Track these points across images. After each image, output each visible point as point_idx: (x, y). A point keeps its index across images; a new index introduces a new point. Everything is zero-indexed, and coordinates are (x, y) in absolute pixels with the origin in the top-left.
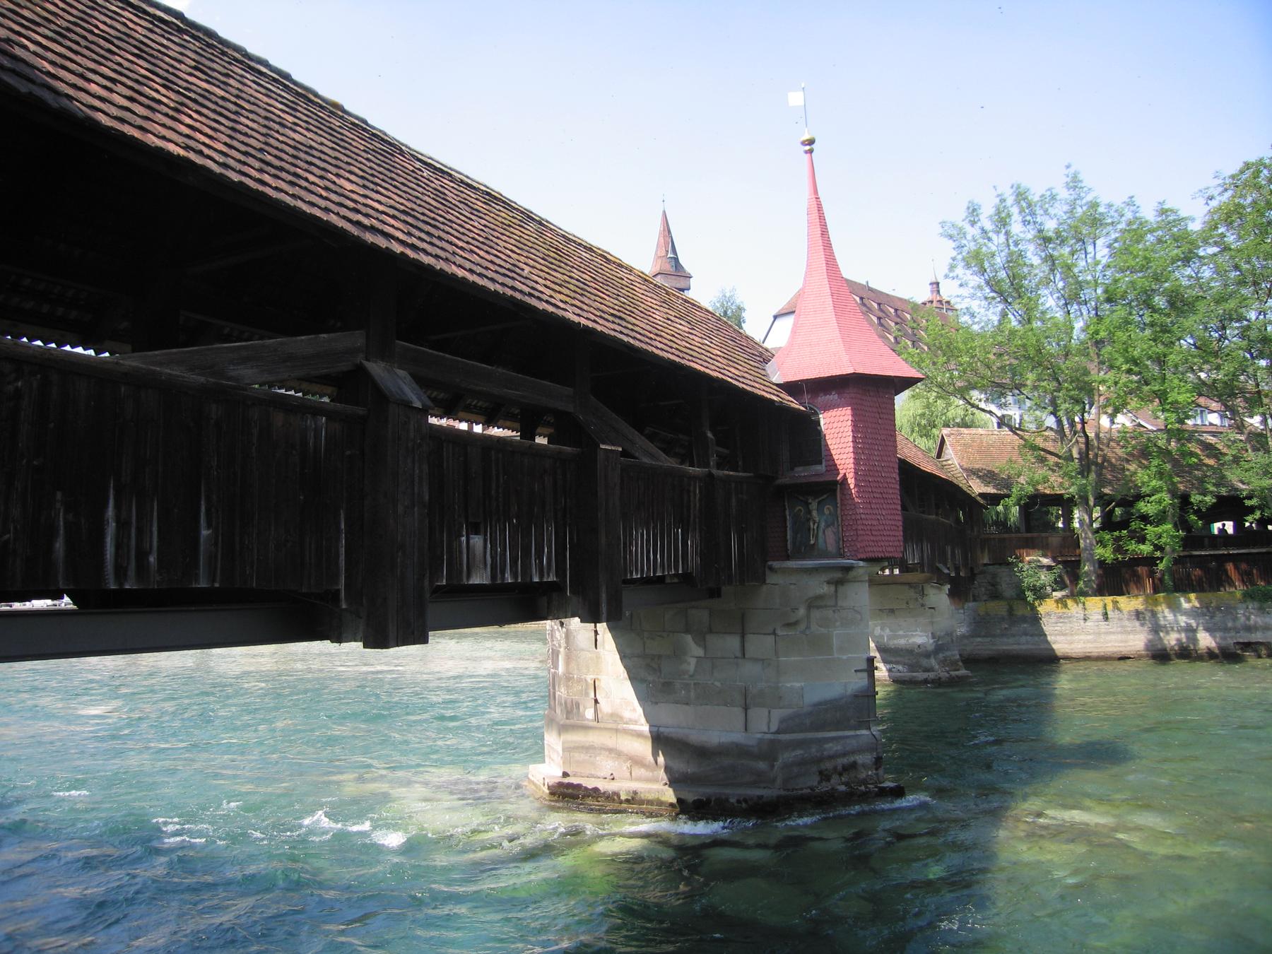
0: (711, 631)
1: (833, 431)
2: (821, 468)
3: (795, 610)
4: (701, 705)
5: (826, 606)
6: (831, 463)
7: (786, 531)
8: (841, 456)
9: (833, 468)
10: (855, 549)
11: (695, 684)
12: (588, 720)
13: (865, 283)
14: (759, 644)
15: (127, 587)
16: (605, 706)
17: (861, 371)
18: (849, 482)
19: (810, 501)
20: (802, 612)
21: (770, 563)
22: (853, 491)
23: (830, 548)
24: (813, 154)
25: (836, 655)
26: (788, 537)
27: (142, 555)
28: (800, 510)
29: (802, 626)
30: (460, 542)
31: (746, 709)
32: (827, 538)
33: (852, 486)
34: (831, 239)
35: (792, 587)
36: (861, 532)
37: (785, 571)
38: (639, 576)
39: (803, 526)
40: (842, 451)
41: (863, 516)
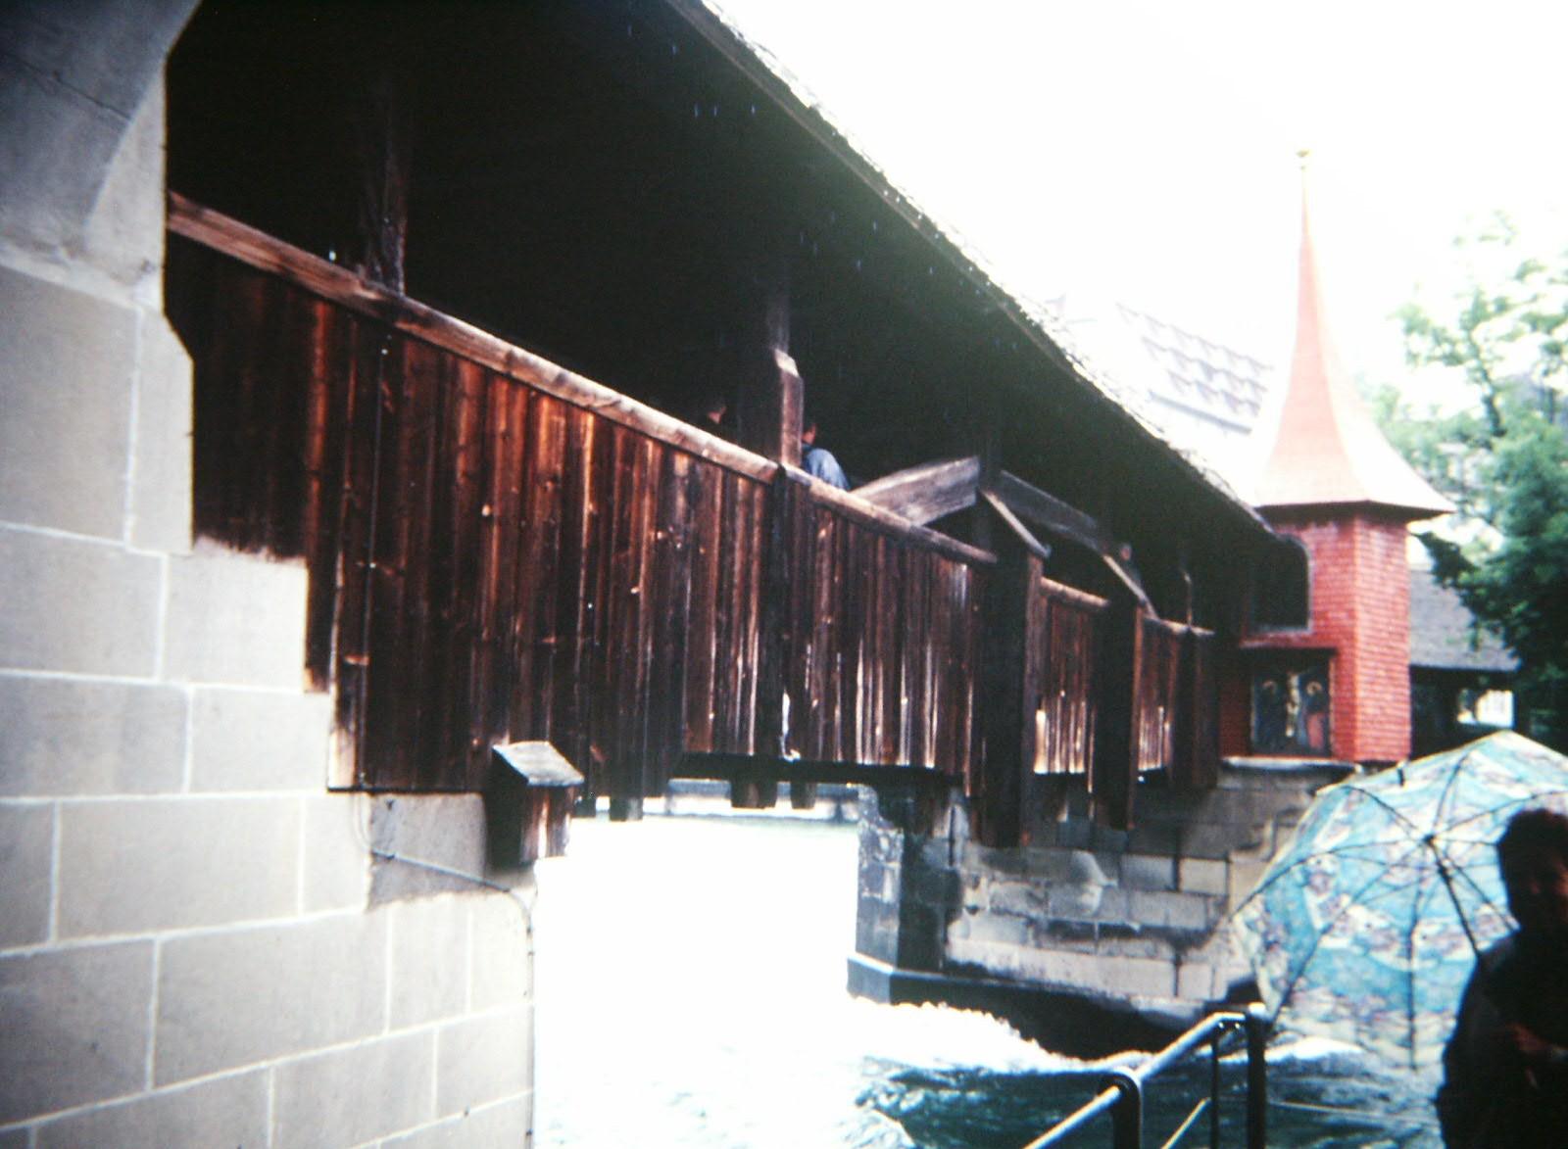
20: (1268, 831)
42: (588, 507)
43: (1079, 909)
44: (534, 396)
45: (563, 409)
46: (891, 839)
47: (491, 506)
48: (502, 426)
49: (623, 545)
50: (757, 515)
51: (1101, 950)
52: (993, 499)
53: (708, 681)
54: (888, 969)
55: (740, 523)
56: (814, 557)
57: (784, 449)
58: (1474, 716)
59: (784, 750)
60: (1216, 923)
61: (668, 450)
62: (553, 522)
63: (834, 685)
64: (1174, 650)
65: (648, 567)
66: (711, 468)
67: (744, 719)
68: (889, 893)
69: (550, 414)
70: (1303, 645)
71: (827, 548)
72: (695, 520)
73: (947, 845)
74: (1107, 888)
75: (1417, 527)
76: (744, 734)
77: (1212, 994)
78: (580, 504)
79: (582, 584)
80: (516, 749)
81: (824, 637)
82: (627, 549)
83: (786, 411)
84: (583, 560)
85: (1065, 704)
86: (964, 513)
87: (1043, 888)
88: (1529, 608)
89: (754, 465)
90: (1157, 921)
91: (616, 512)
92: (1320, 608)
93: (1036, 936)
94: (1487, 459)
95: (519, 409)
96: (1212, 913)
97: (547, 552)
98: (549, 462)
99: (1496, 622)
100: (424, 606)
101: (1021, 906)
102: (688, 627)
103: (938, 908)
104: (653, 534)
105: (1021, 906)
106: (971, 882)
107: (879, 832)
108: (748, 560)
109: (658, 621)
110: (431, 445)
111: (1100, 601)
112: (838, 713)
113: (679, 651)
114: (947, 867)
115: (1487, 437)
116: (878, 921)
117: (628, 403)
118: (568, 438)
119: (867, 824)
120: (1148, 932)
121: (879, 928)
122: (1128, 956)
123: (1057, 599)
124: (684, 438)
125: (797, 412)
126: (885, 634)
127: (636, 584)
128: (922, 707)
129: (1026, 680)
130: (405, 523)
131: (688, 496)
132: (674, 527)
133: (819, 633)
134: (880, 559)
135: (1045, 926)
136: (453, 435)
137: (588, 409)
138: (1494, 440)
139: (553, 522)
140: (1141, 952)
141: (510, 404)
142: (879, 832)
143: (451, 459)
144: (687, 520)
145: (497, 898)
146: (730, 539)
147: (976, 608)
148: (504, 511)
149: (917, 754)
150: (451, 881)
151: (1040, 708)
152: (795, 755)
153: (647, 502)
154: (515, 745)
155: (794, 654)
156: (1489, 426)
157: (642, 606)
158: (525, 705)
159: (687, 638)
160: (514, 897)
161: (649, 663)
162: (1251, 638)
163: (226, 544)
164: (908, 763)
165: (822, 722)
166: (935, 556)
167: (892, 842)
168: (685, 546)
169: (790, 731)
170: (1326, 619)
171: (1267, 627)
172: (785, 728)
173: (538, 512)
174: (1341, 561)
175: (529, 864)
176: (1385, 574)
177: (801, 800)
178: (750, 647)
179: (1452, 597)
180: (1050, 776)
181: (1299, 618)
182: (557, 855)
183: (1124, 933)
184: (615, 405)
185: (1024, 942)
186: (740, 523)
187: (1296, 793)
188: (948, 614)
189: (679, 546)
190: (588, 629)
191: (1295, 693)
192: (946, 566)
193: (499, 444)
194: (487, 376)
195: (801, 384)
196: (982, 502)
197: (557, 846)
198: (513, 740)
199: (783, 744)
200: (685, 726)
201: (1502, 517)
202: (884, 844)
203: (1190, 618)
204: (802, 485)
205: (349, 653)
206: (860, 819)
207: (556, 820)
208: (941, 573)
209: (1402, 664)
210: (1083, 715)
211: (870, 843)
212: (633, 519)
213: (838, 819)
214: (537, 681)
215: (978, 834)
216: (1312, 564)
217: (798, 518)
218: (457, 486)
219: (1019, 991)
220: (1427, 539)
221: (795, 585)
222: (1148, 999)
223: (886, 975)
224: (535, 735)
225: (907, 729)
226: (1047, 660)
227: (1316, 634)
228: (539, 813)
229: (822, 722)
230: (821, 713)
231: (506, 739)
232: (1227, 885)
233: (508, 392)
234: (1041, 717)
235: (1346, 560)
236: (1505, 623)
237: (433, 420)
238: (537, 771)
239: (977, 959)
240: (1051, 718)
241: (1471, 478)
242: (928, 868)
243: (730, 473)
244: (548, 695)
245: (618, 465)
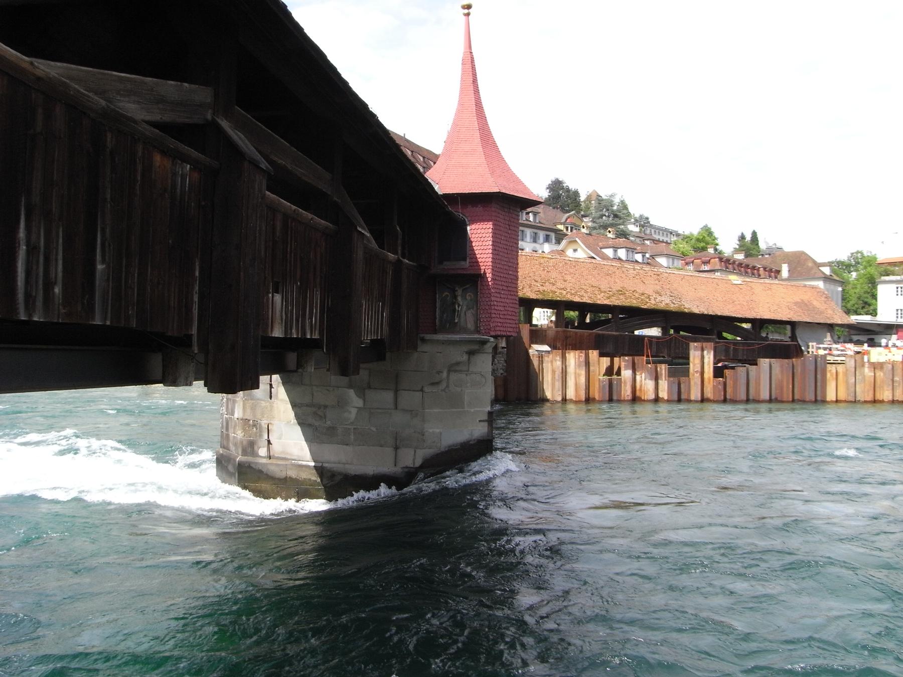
0: (369, 387)
1: (477, 236)
2: (466, 264)
3: (439, 372)
4: (359, 445)
5: (461, 371)
6: (474, 260)
7: (435, 311)
8: (482, 256)
9: (475, 264)
10: (489, 327)
11: (354, 429)
12: (261, 457)
13: (403, 136)
14: (409, 399)
15: (36, 319)
16: (276, 448)
17: (504, 191)
18: (488, 276)
19: (457, 289)
20: (445, 374)
21: (422, 335)
22: (490, 283)
24: (470, 17)
25: (466, 409)
27: (48, 286)
28: (448, 295)
29: (444, 385)
30: (268, 298)
31: (396, 448)
32: (467, 319)
33: (489, 279)
34: (479, 86)
35: (439, 354)
36: (494, 316)
37: (432, 341)
38: (375, 338)
40: (484, 252)
41: (495, 303)
163: (17, 254)
180: (311, 339)
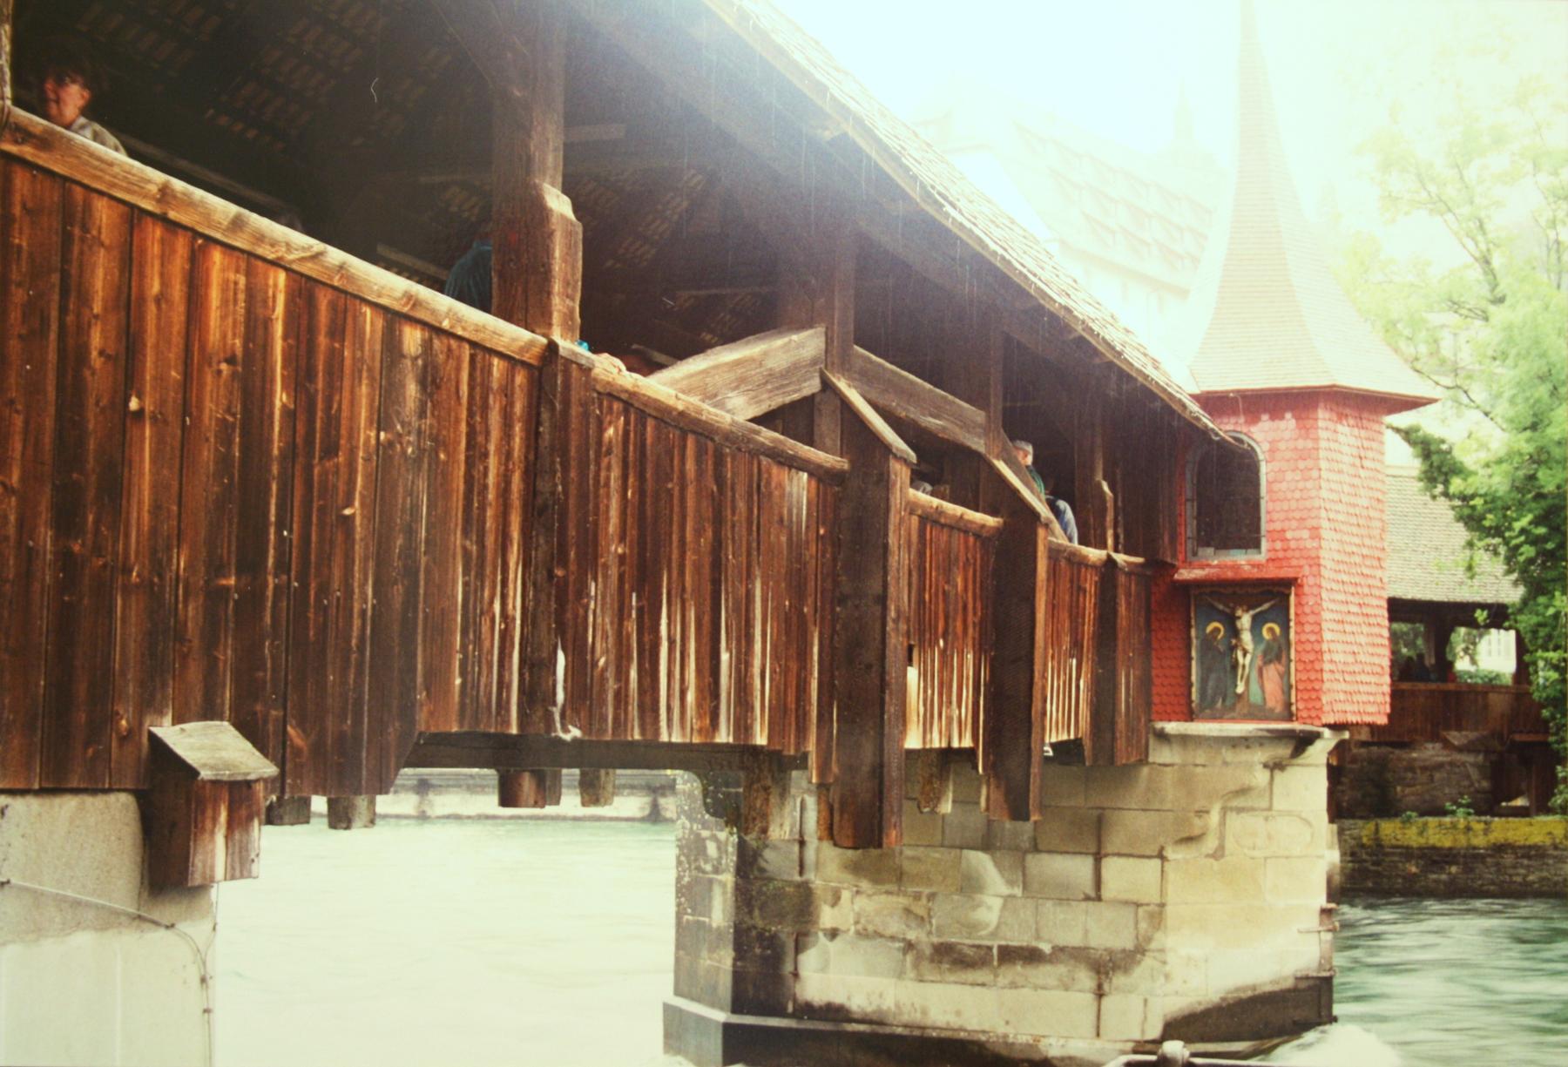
0: (1036, 849)
5: (1252, 809)
19: (1239, 613)
20: (1214, 817)
23: (1271, 703)
26: (1194, 678)
35: (1199, 770)
39: (1223, 660)
42: (280, 398)
43: (973, 927)
44: (201, 244)
45: (243, 265)
46: (721, 841)
47: (140, 397)
48: (155, 287)
49: (331, 450)
50: (518, 408)
51: (1002, 981)
52: (842, 384)
53: (453, 633)
54: (721, 1016)
55: (495, 418)
56: (598, 464)
57: (556, 318)
58: (1473, 662)
59: (558, 725)
60: (1149, 939)
61: (394, 318)
62: (230, 419)
63: (629, 636)
64: (1090, 583)
65: (367, 476)
66: (454, 344)
67: (503, 685)
68: (720, 912)
69: (223, 270)
70: (1256, 574)
71: (617, 451)
72: (433, 414)
73: (796, 848)
74: (1008, 899)
75: (1403, 419)
76: (503, 706)
77: (1143, 1032)
78: (272, 393)
79: (273, 501)
80: (183, 730)
81: (614, 572)
82: (337, 455)
83: (558, 266)
84: (275, 469)
85: (943, 653)
86: (808, 401)
87: (924, 901)
88: (1536, 522)
89: (514, 340)
90: (1073, 939)
91: (320, 406)
92: (1278, 526)
93: (916, 965)
94: (1487, 335)
95: (179, 263)
96: (1143, 925)
97: (224, 461)
98: (224, 337)
99: (1497, 540)
100: (46, 538)
101: (895, 926)
102: (423, 560)
103: (785, 932)
104: (373, 434)
105: (895, 926)
106: (829, 897)
107: (705, 833)
108: (507, 470)
109: (381, 560)
110: (54, 314)
111: (991, 521)
112: (633, 674)
113: (411, 593)
114: (797, 878)
115: (1484, 304)
116: (705, 954)
117: (335, 255)
118: (249, 311)
119: (688, 824)
120: (1060, 953)
121: (706, 961)
122: (1036, 988)
123: (929, 519)
124: (416, 303)
125: (574, 267)
126: (697, 568)
127: (349, 504)
128: (748, 665)
129: (890, 626)
130: (19, 421)
131: (422, 383)
132: (403, 424)
133: (606, 567)
134: (690, 466)
135: (928, 951)
136: (85, 299)
137: (276, 264)
138: (1492, 309)
139: (230, 419)
140: (1052, 982)
141: (165, 259)
142: (705, 833)
143: (82, 330)
144: (422, 414)
145: (157, 937)
146: (480, 439)
147: (822, 532)
148: (162, 403)
149: (743, 726)
150: (90, 914)
151: (911, 665)
152: (575, 732)
153: (364, 389)
154: (178, 727)
155: (571, 597)
156: (1485, 291)
157: (359, 532)
158: (194, 673)
159: (422, 576)
160: (184, 936)
161: (369, 613)
162: (1190, 566)
164: (731, 740)
165: (612, 685)
166: (765, 461)
167: (721, 847)
168: (420, 450)
169: (565, 700)
170: (1284, 540)
171: (1210, 551)
172: (560, 696)
173: (209, 405)
174: (1302, 465)
175: (203, 889)
176: (1356, 481)
177: (592, 792)
178: (511, 586)
179: (1443, 510)
181: (1251, 540)
182: (242, 877)
183: (1031, 956)
184: (316, 257)
185: (900, 975)
186: (495, 418)
187: (1249, 767)
188: (784, 539)
189: (410, 450)
190: (282, 566)
191: (1246, 637)
192: (778, 474)
193: (152, 309)
194: (133, 217)
195: (579, 229)
196: (827, 385)
197: (241, 866)
198: (178, 719)
199: (557, 717)
200: (421, 696)
201: (1502, 409)
202: (712, 849)
203: (1110, 542)
204: (580, 366)
205: (785, 1008)
206: (679, 818)
207: (238, 823)
208: (773, 485)
209: (1380, 598)
210: (969, 671)
211: (691, 850)
212: (345, 414)
213: (655, 816)
214: (211, 641)
215: (830, 832)
216: (1264, 468)
217: (575, 411)
218: (90, 367)
219: (893, 1037)
220: (1408, 435)
221: (572, 502)
222: (1062, 1042)
223: (717, 1022)
224: (209, 712)
225: (729, 694)
226: (921, 601)
227: (1270, 560)
228: (215, 820)
229: (612, 685)
230: (610, 675)
231: (168, 719)
232: (1162, 892)
233: (163, 241)
234: (912, 674)
235: (1309, 463)
236: (1506, 542)
237: (55, 278)
238: (212, 762)
239: (838, 998)
240: (923, 675)
241: (1466, 358)
242: (771, 879)
243: (481, 350)
244: (227, 654)
245: (322, 340)
